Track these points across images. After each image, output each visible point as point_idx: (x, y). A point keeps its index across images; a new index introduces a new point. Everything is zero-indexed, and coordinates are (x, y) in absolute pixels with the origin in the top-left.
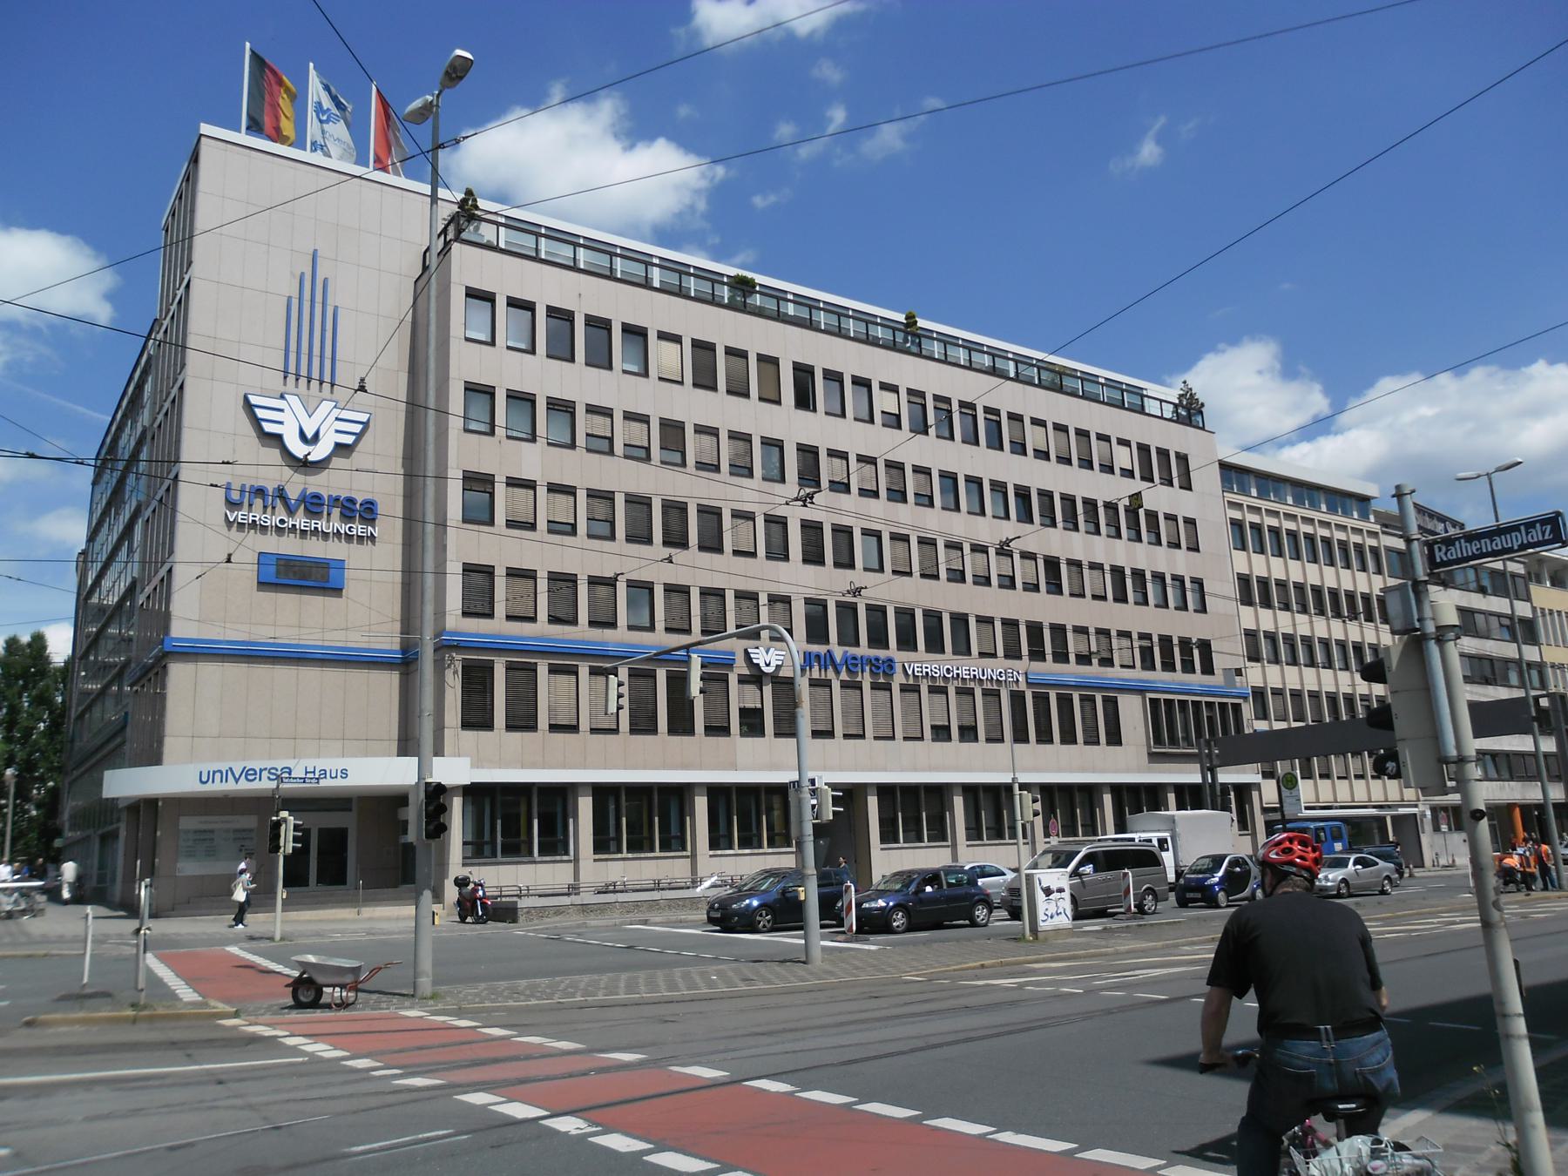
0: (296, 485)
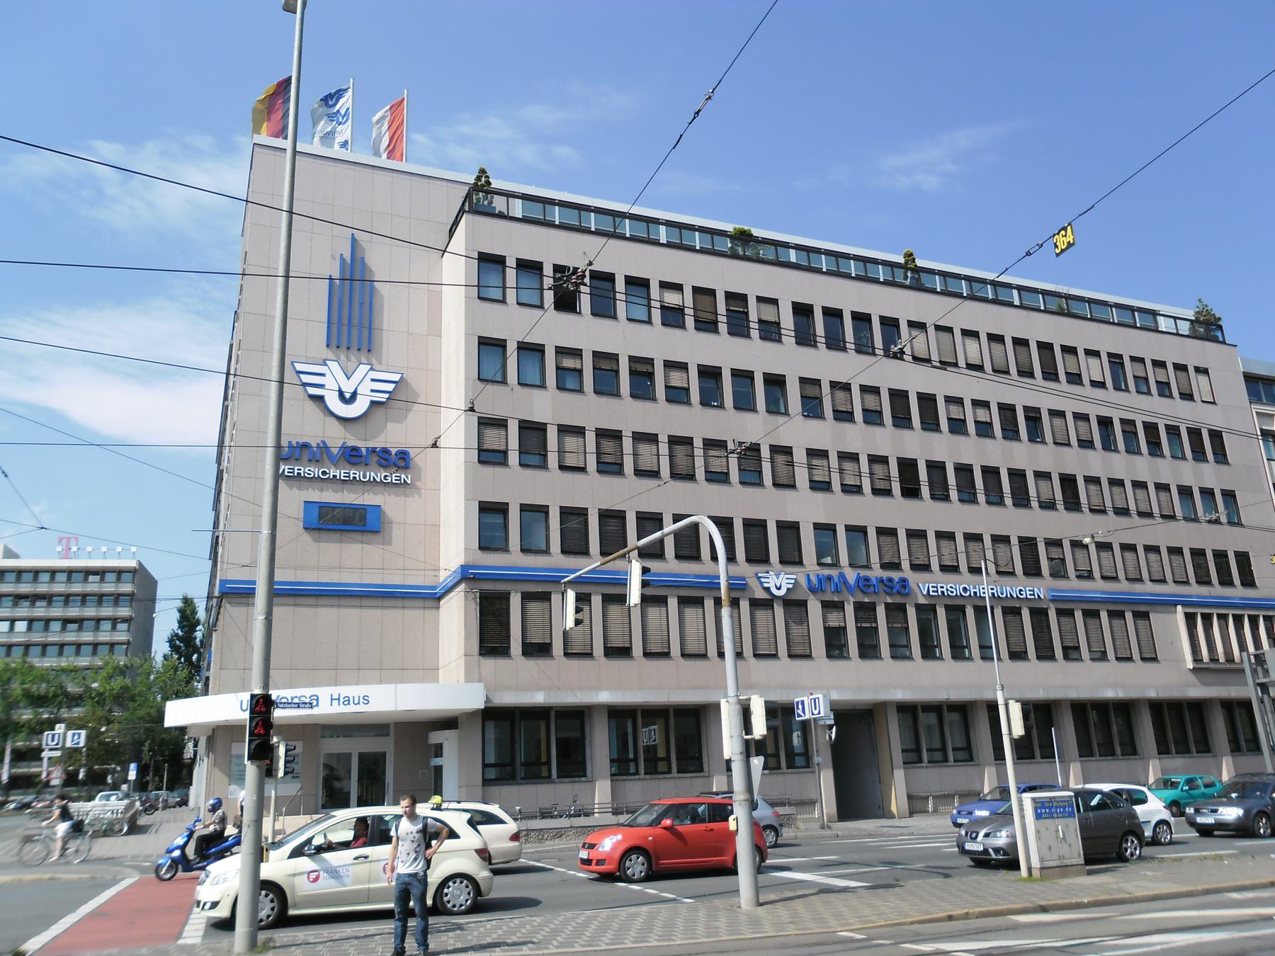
0: (337, 437)
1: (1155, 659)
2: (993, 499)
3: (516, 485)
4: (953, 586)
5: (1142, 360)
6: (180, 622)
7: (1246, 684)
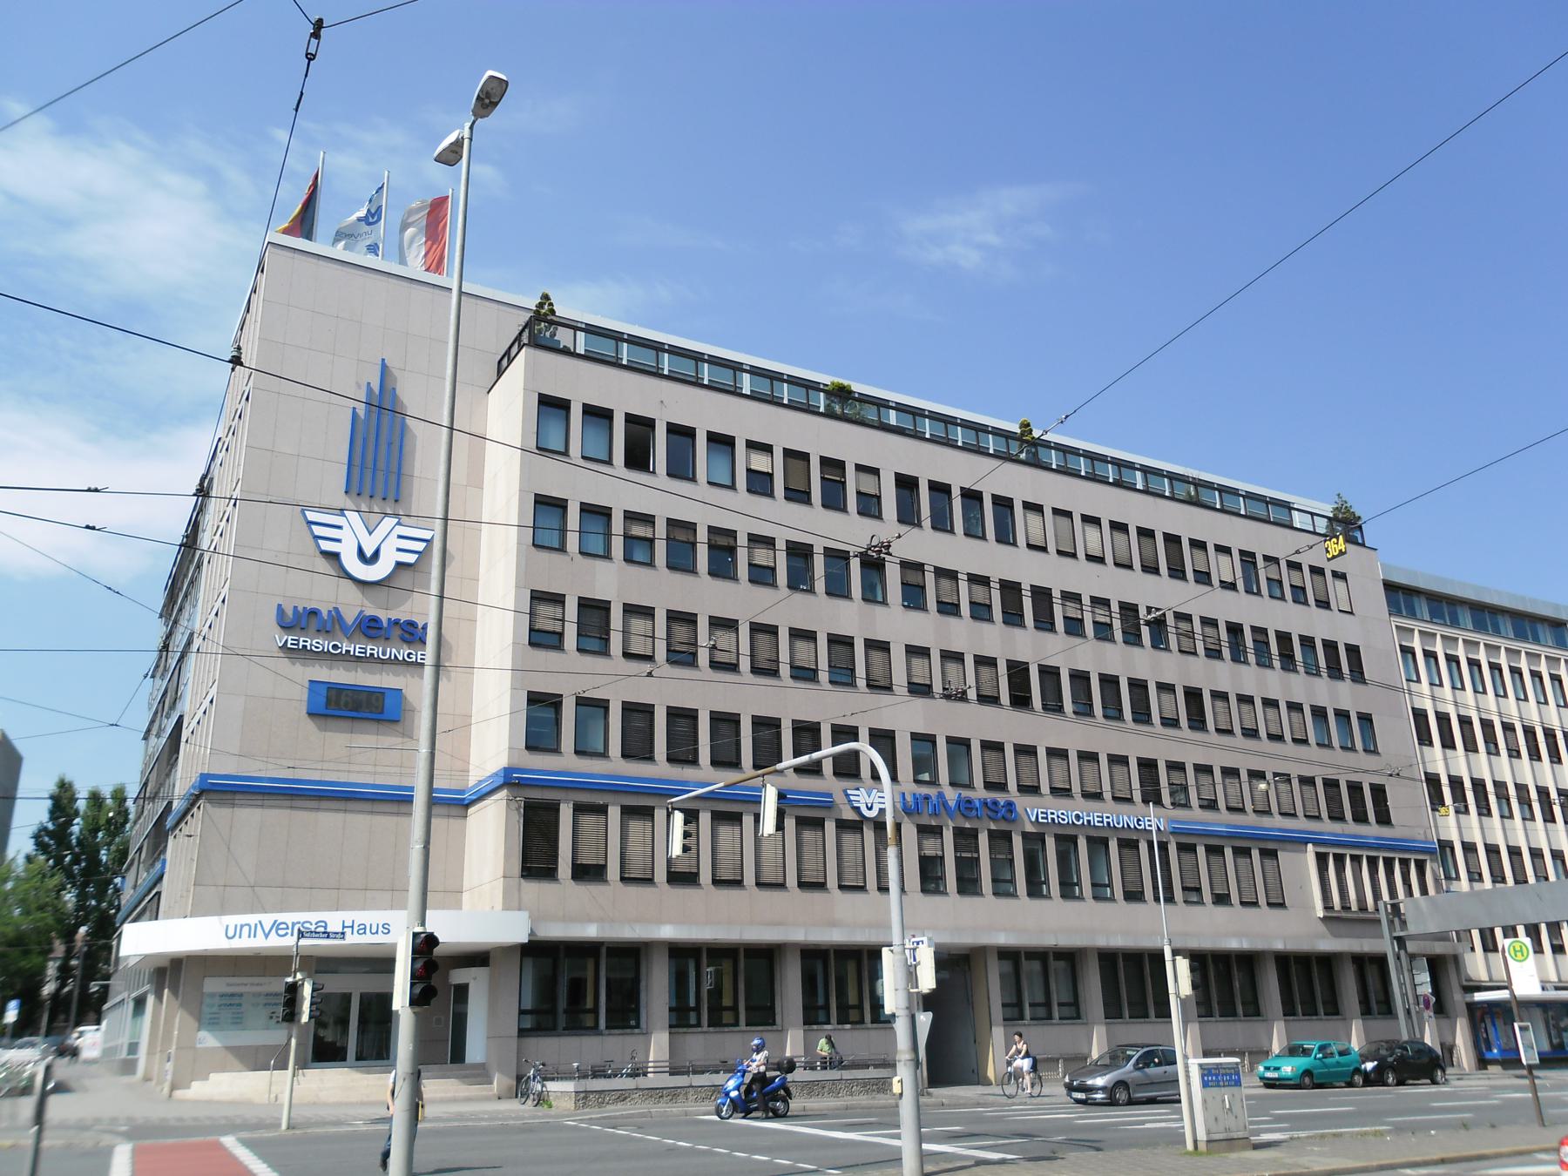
0: (353, 605)
1: (1282, 905)
2: (1111, 713)
3: (572, 673)
4: (1067, 812)
5: (1276, 560)
6: (52, 812)
7: (1382, 937)
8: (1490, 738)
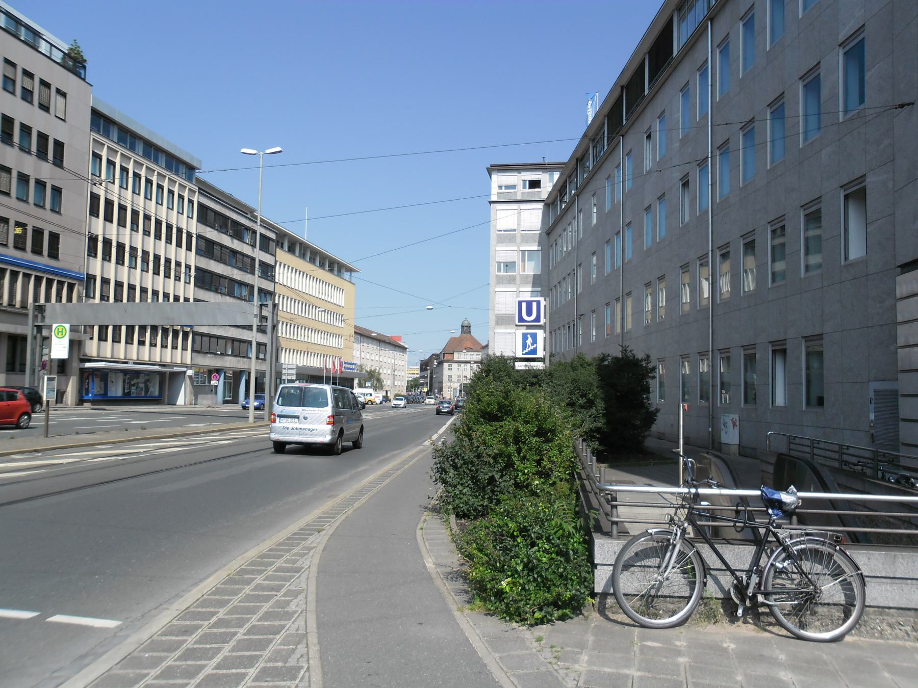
7: (27, 325)
8: (135, 222)
